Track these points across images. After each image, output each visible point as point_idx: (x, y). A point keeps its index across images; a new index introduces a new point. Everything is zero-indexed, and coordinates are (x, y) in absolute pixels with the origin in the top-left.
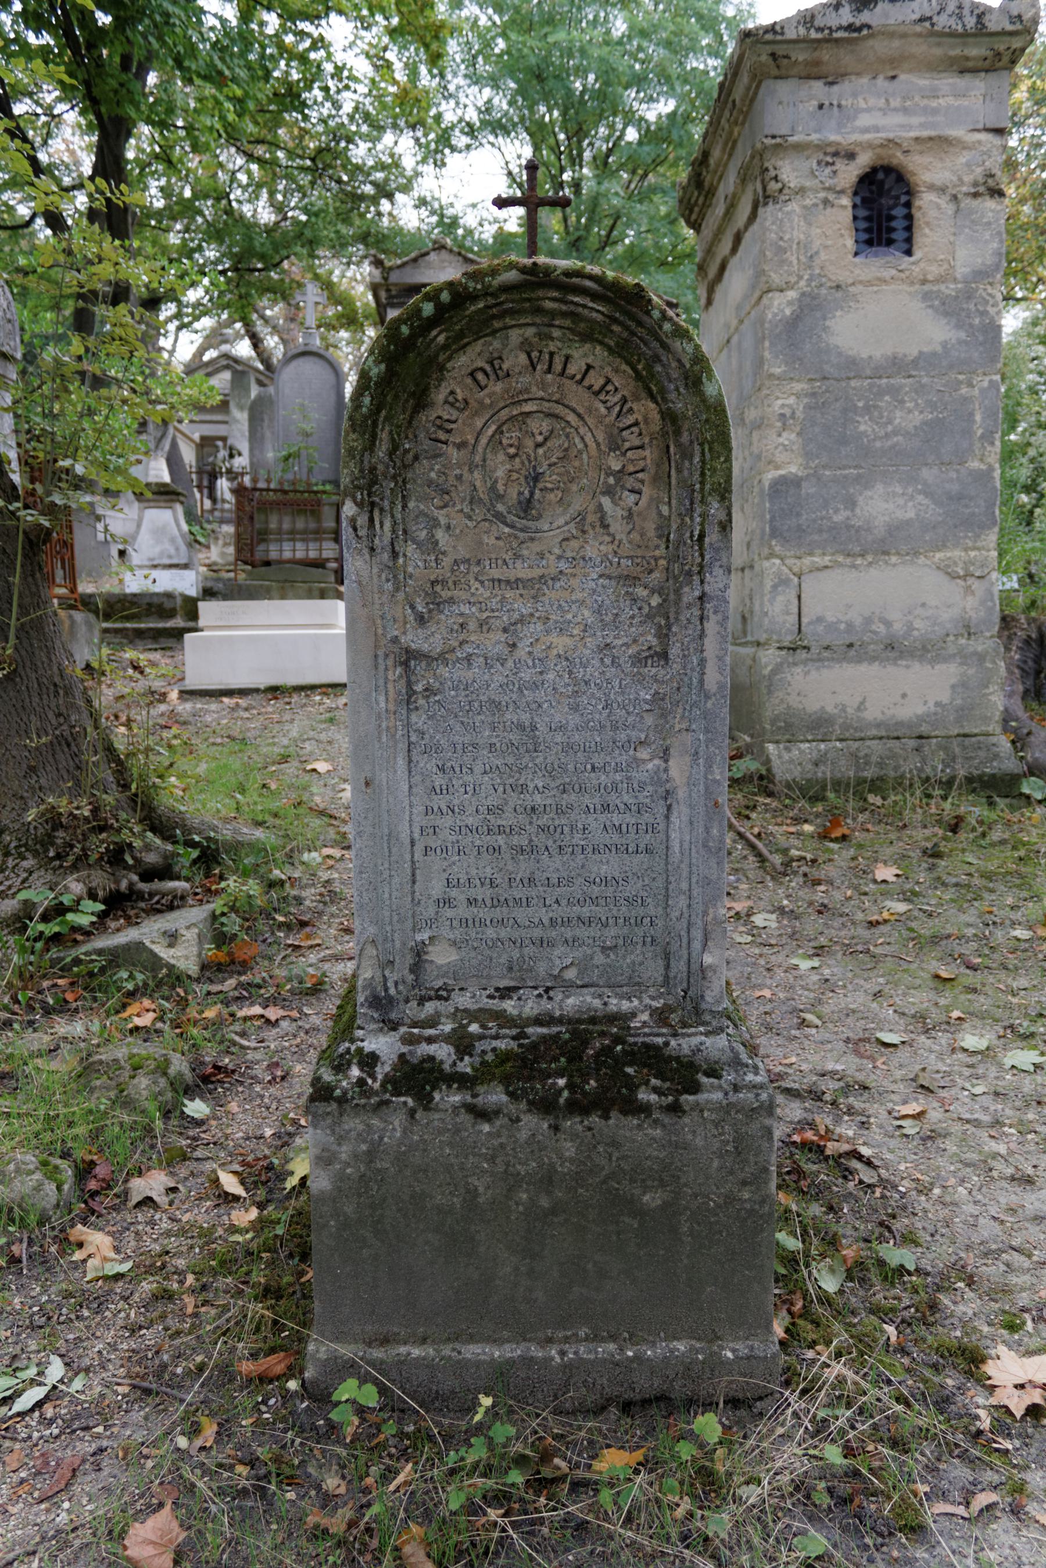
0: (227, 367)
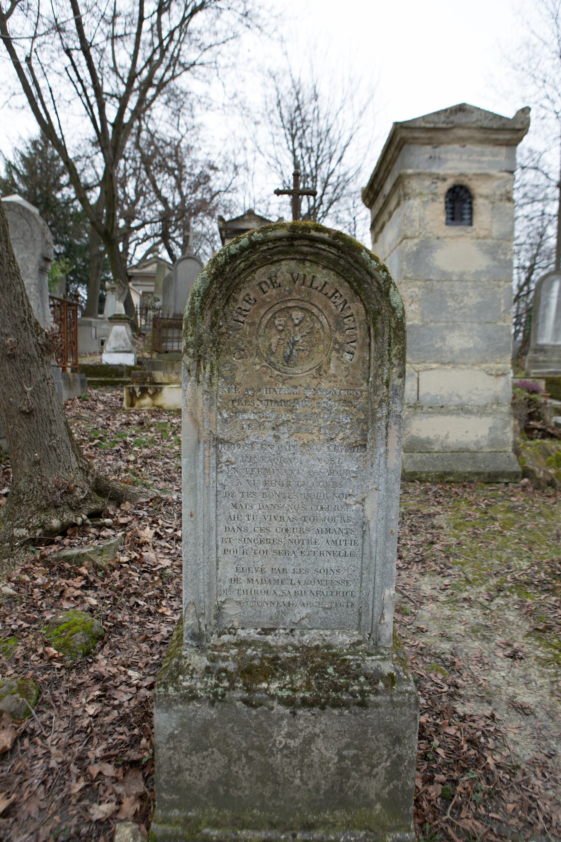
0: (156, 262)
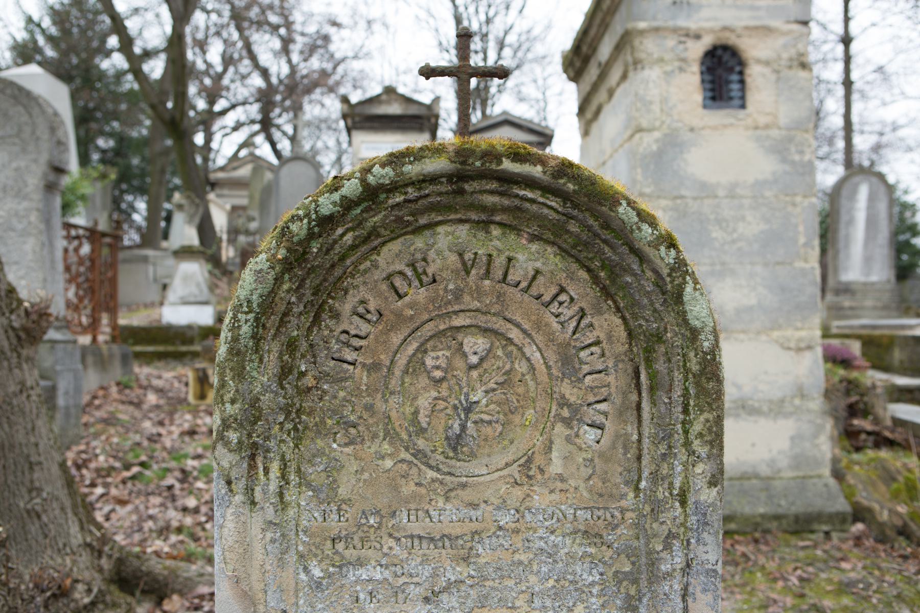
0: (252, 161)
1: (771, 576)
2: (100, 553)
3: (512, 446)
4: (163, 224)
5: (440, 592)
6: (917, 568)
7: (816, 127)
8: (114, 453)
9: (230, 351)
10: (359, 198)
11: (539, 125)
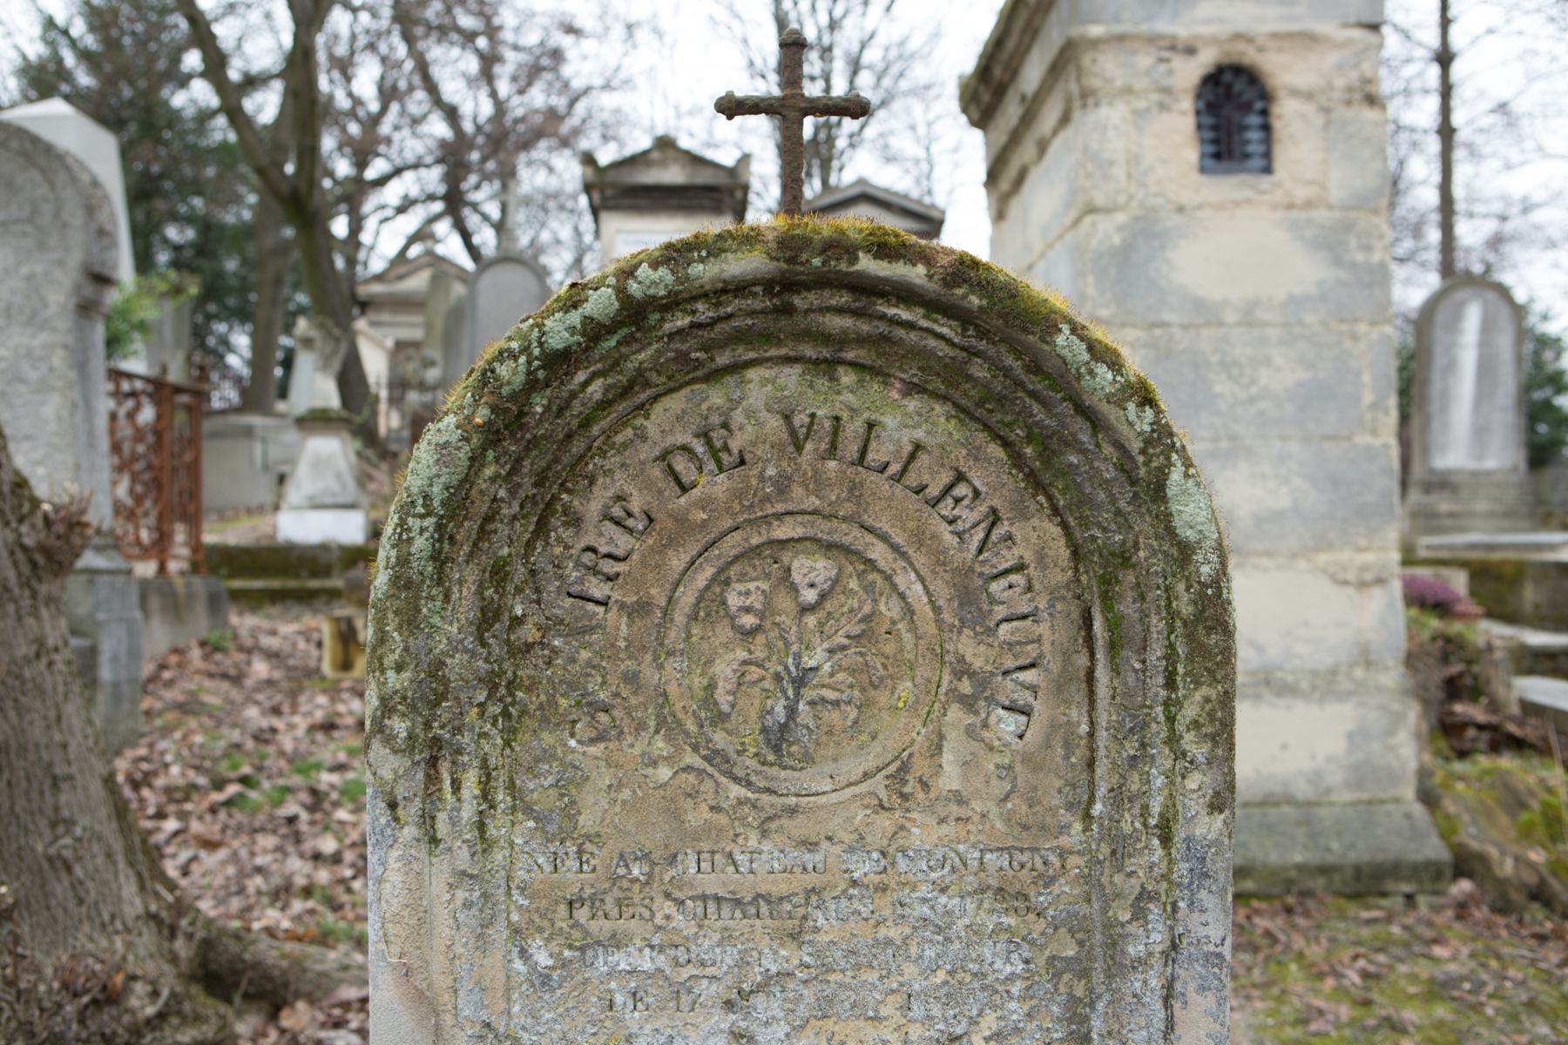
0: (430, 265)
1: (1314, 970)
2: (173, 931)
3: (874, 743)
4: (278, 372)
5: (752, 992)
6: (1561, 956)
7: (1392, 205)
8: (197, 762)
9: (395, 581)
10: (613, 320)
11: (919, 202)
